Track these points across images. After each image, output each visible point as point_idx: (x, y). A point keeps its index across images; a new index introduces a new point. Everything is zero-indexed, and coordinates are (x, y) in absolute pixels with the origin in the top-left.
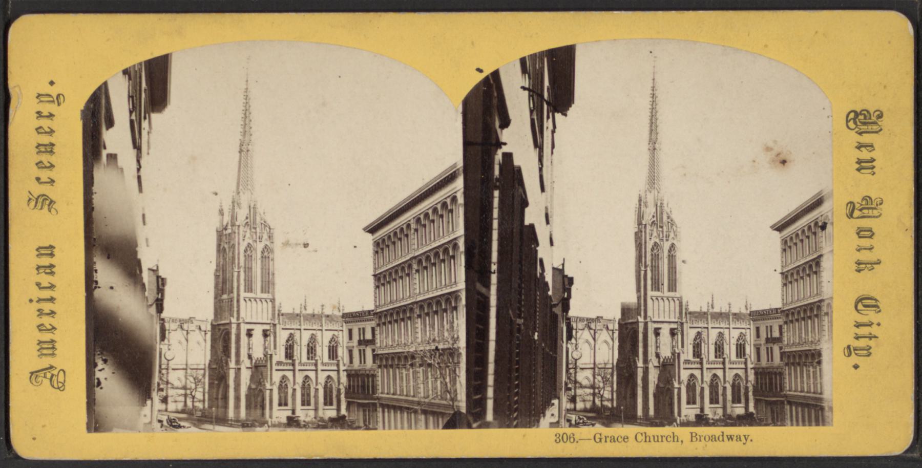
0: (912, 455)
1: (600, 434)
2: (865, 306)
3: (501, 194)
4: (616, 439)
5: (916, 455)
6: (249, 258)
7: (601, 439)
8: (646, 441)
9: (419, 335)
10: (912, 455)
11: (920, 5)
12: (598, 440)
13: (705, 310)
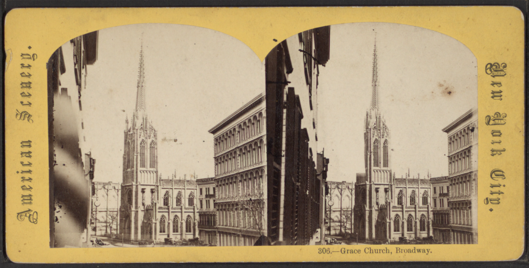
1: (345, 249)
5: (526, 260)
6: (143, 148)
7: (345, 252)
11: (528, 3)
12: (343, 252)
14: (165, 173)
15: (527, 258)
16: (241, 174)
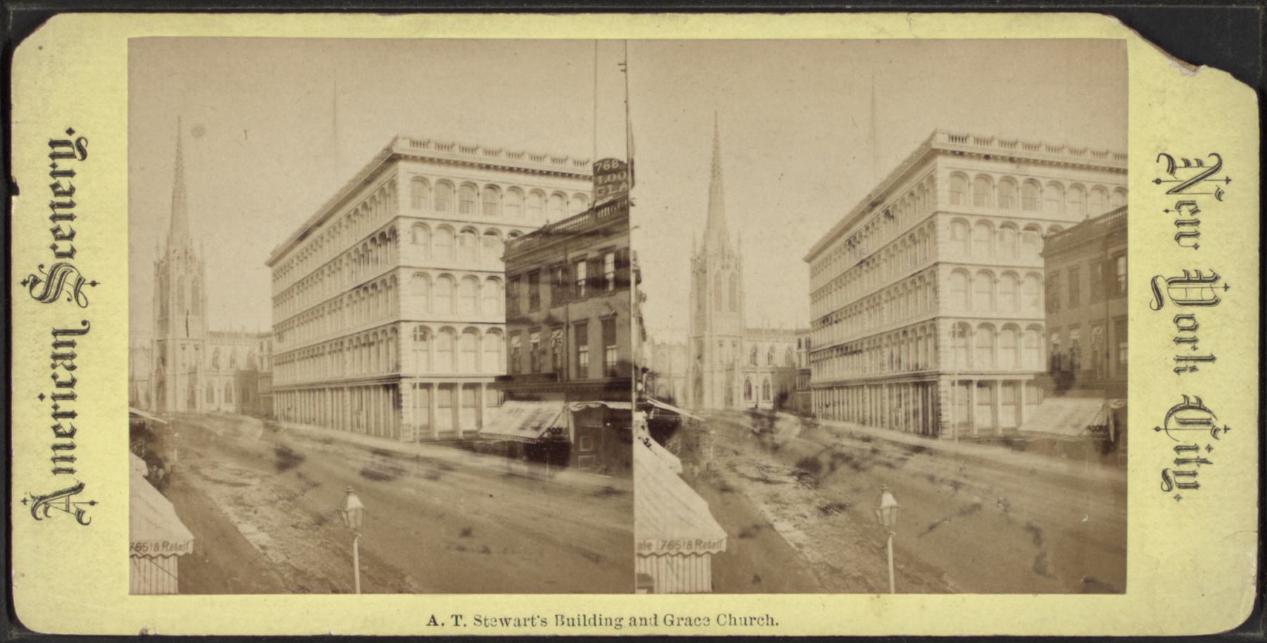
0: (1252, 634)
1: (672, 616)
2: (1184, 423)
3: (5, 27)
4: (693, 622)
5: (1260, 634)
6: (718, 283)
7: (672, 622)
8: (730, 624)
9: (886, 318)
10: (1252, 634)
11: (1263, 16)
12: (668, 623)
13: (760, 327)
14: (753, 322)
15: (1261, 628)
16: (298, 316)
